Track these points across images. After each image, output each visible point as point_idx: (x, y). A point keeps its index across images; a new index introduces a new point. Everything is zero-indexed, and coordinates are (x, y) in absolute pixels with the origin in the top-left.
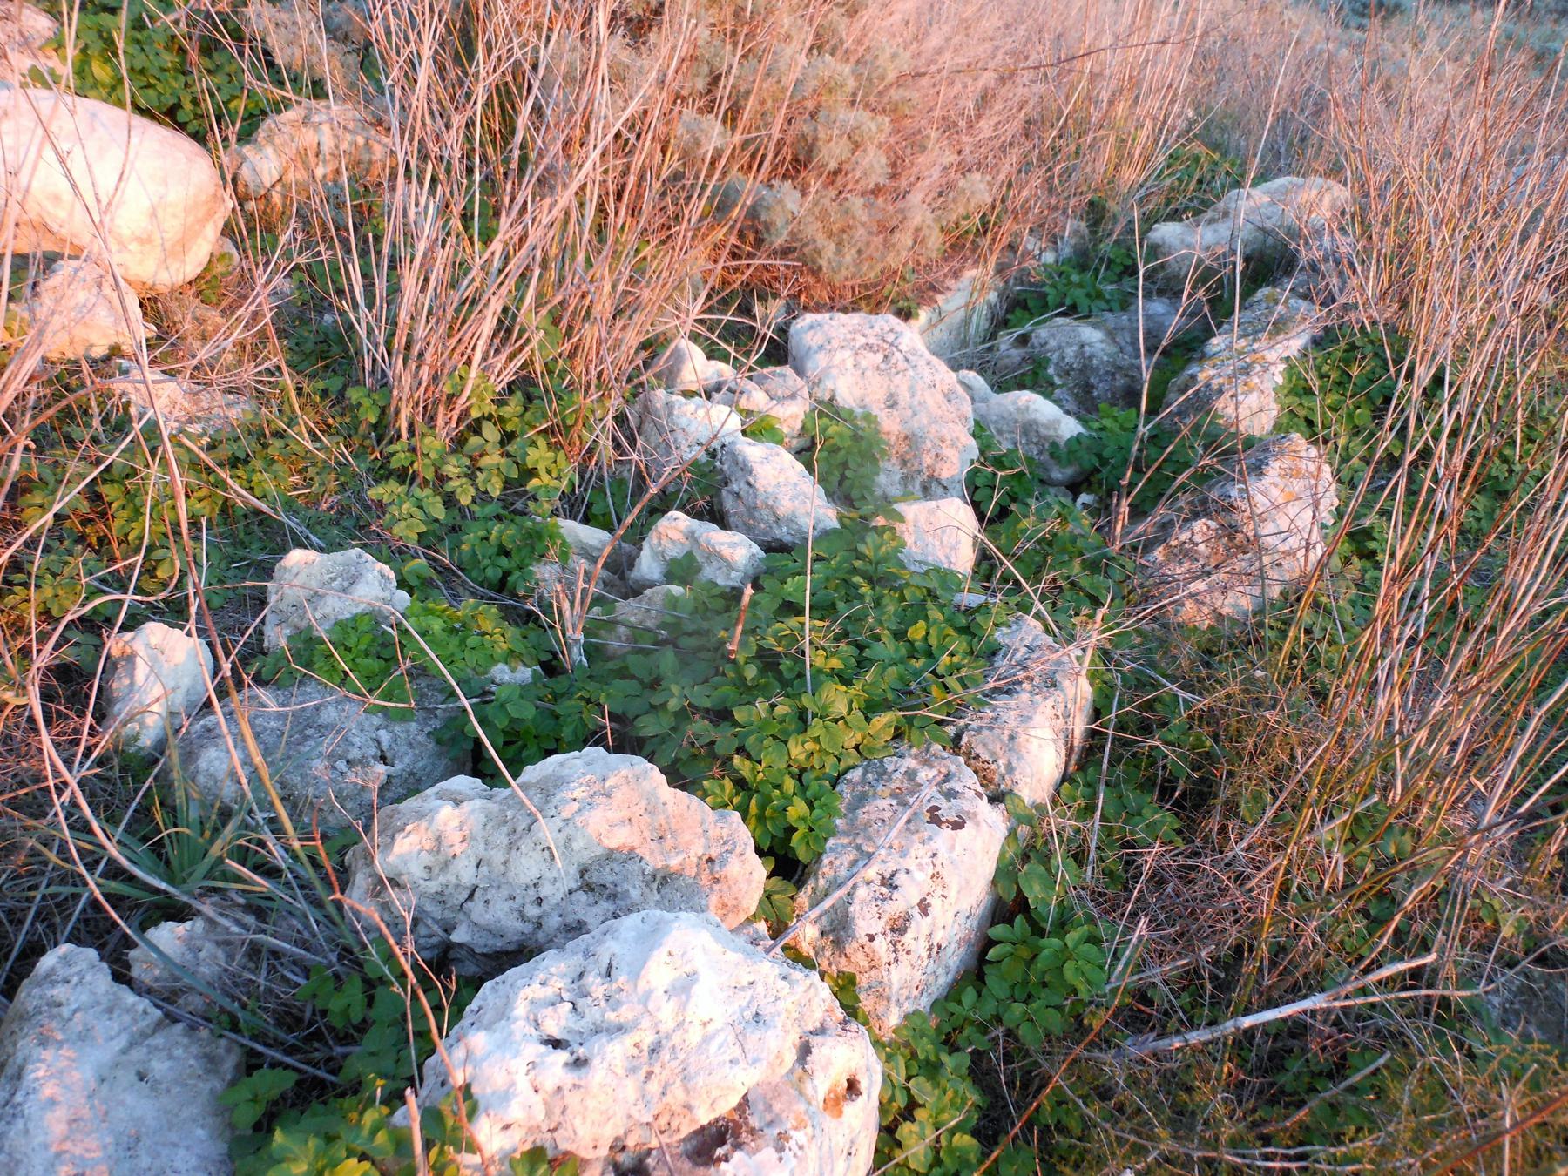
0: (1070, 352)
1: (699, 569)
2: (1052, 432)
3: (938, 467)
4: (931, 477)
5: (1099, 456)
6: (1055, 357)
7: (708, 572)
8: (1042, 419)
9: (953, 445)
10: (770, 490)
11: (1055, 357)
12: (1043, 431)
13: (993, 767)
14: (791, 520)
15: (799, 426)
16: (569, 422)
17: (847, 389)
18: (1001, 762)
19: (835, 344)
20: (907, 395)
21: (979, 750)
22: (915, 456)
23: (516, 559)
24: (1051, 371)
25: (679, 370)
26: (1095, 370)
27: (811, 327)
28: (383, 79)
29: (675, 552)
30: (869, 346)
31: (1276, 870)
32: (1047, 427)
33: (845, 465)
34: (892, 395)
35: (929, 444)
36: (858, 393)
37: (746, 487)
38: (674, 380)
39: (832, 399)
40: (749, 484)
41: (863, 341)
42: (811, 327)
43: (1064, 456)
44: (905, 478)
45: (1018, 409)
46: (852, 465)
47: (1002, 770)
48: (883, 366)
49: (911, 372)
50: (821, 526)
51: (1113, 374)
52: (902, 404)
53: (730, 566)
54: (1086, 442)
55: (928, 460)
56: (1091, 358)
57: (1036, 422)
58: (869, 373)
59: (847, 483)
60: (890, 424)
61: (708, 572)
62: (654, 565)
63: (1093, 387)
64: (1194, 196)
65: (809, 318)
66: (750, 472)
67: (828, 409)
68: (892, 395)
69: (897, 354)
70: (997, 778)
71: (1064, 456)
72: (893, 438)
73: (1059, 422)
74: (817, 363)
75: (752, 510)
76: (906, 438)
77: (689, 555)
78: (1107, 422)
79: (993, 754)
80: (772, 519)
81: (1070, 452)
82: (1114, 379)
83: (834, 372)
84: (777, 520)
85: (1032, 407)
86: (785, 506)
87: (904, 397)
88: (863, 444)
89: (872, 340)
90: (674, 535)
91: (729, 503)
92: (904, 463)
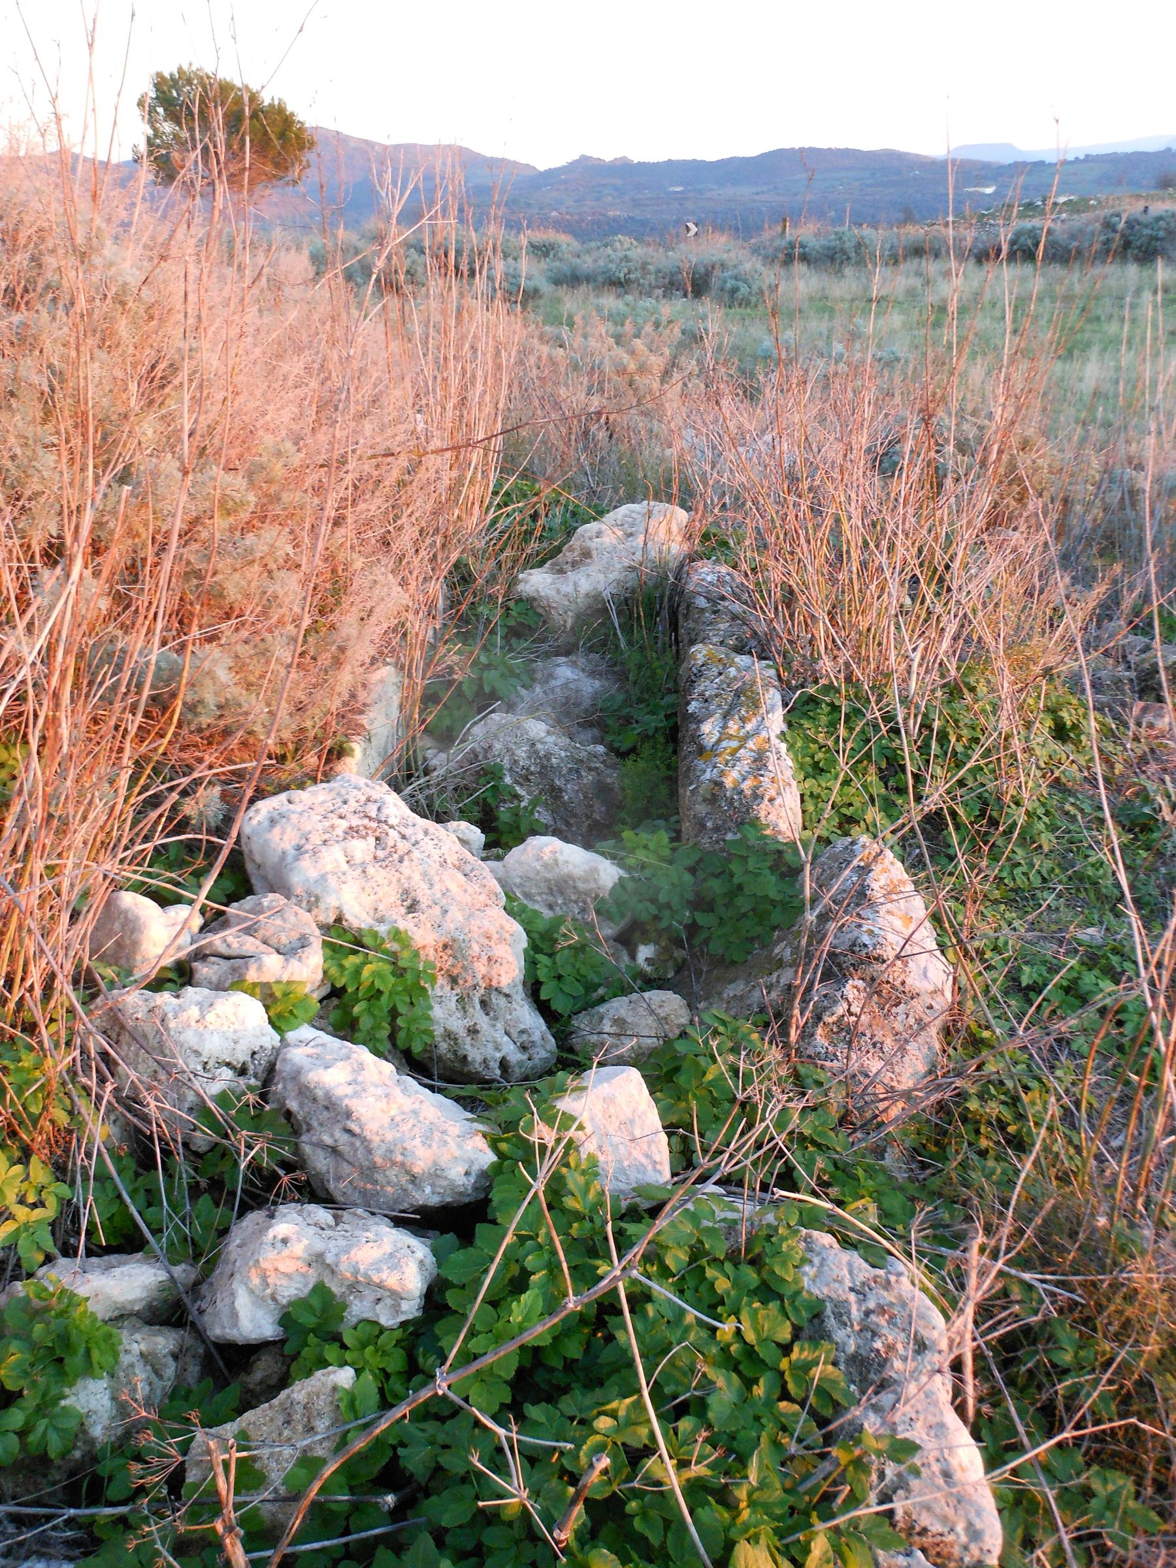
0: (521, 753)
1: (344, 1306)
2: (592, 885)
3: (494, 973)
4: (489, 988)
5: (654, 901)
6: (506, 763)
7: (359, 1309)
8: (578, 872)
9: (502, 940)
10: (389, 1137)
11: (506, 763)
12: (581, 886)
13: (950, 1538)
14: (436, 1174)
15: (320, 975)
16: (35, 1110)
17: (357, 904)
18: (960, 1528)
19: (316, 839)
20: (425, 886)
21: (925, 1520)
22: (464, 968)
23: (31, 1399)
24: (508, 780)
25: (135, 944)
26: (556, 770)
27: (273, 822)
28: (79, 1059)
29: (290, 1290)
30: (352, 831)
31: (140, 794)
32: (586, 881)
33: (394, 1013)
34: (406, 892)
35: (476, 948)
36: (368, 900)
37: (345, 1137)
38: (130, 957)
39: (339, 920)
40: (349, 1131)
41: (344, 824)
42: (273, 822)
43: (614, 909)
44: (461, 1000)
45: (545, 866)
46: (402, 1009)
47: (964, 1539)
48: (381, 854)
49: (416, 854)
50: (475, 1169)
51: (577, 771)
52: (424, 902)
53: (397, 1297)
54: (630, 886)
55: (481, 968)
56: (548, 756)
57: (570, 877)
58: (371, 870)
59: (401, 1035)
60: (424, 935)
61: (359, 1309)
62: (260, 1313)
63: (560, 790)
64: (549, 542)
65: (265, 807)
66: (348, 1115)
67: (343, 939)
68: (406, 892)
69: (391, 832)
70: (957, 1551)
71: (614, 909)
72: (431, 952)
73: (596, 870)
74: (304, 873)
75: (369, 1171)
76: (445, 946)
77: (320, 1289)
78: (641, 855)
79: (944, 1519)
80: (404, 1179)
81: (617, 903)
82: (580, 776)
83: (332, 881)
84: (414, 1179)
85: (561, 858)
86: (422, 1159)
87: (423, 894)
88: (409, 976)
89: (355, 821)
90: (288, 1266)
91: (320, 1162)
92: (454, 980)
